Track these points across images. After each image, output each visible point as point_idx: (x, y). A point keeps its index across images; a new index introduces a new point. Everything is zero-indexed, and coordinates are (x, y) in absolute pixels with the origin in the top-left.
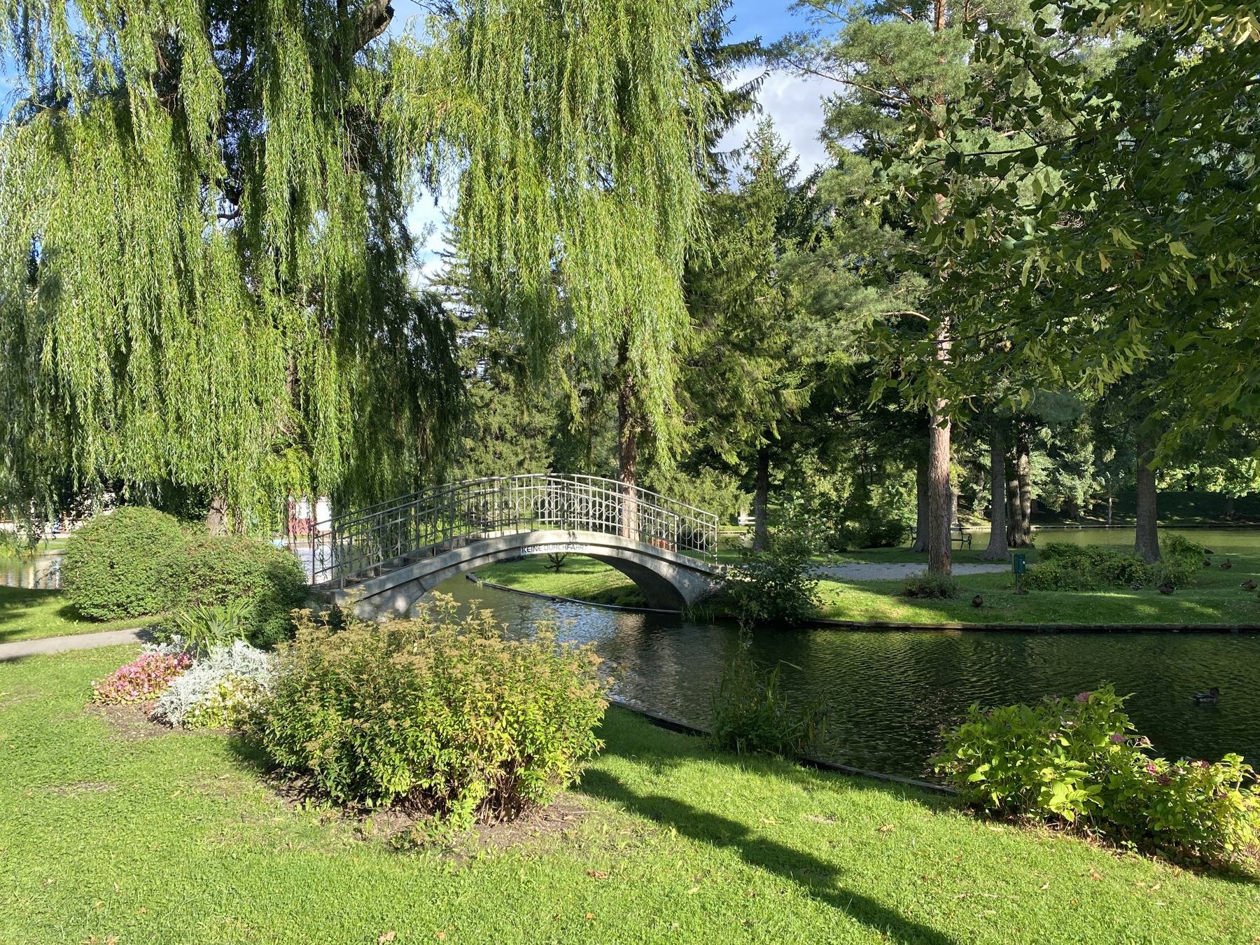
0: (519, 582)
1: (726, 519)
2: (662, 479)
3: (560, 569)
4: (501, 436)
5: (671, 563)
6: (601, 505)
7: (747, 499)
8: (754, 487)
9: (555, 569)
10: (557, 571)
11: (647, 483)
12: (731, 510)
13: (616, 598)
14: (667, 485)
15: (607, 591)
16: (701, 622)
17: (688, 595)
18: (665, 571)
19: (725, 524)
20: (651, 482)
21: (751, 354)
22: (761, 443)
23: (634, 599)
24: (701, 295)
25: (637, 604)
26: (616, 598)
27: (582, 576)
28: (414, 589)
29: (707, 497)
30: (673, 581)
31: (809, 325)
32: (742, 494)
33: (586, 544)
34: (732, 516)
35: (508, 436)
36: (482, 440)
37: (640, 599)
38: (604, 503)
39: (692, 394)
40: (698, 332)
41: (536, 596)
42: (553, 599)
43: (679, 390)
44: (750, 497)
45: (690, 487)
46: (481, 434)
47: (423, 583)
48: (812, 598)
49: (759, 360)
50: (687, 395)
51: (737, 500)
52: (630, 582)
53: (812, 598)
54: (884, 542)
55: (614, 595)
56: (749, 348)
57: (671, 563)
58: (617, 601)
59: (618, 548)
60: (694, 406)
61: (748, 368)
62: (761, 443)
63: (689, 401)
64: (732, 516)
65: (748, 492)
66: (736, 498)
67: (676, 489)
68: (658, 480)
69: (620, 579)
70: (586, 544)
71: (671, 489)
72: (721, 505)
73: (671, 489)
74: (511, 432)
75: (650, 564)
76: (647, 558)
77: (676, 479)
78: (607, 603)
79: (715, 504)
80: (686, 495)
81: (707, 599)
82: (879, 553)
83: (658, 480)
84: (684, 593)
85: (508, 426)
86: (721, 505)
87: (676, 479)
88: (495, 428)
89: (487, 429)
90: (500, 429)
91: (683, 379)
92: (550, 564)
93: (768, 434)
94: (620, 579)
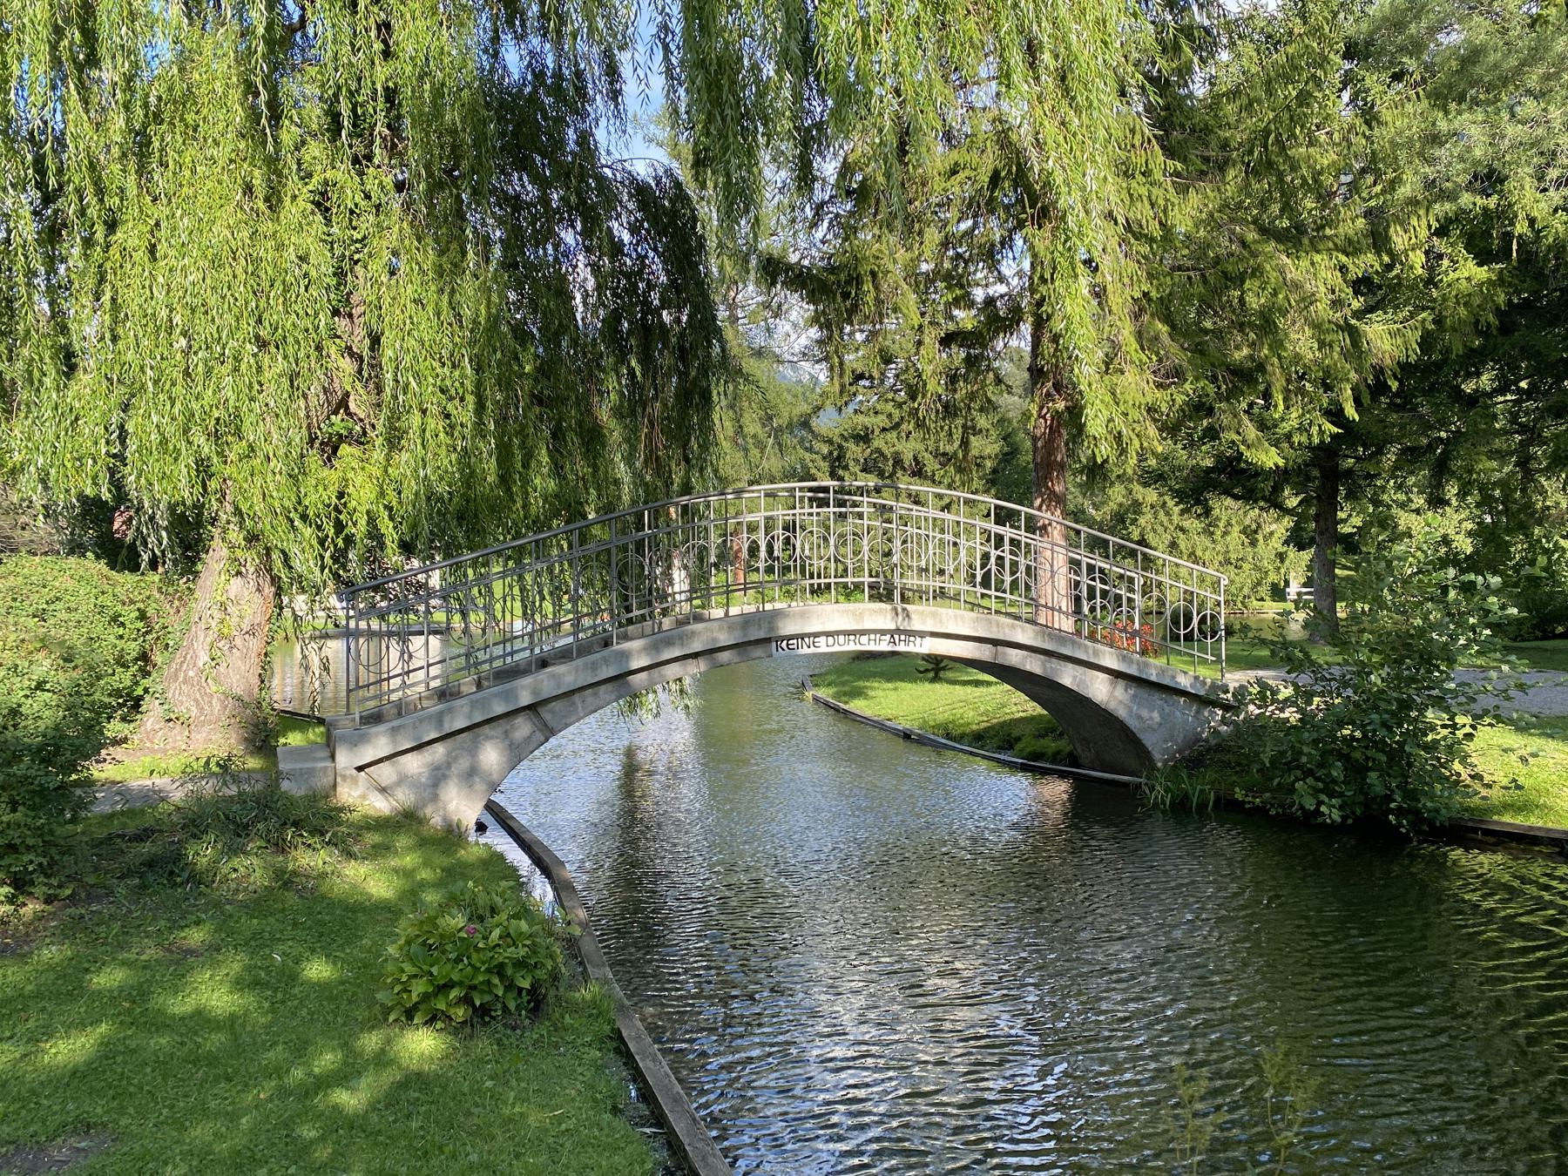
0: (866, 697)
1: (1264, 591)
2: (1160, 530)
3: (942, 674)
4: (918, 472)
5: (1116, 675)
6: (1014, 564)
7: (1299, 562)
8: (1312, 542)
9: (931, 675)
10: (936, 679)
11: (1136, 536)
12: (1272, 577)
13: (1018, 739)
14: (1167, 538)
15: (1003, 725)
16: (1182, 811)
17: (1160, 747)
18: (1099, 689)
19: (1262, 599)
20: (1142, 535)
21: (1298, 245)
22: (1321, 432)
23: (1050, 745)
24: (1193, 131)
25: (1056, 758)
26: (1018, 739)
27: (969, 689)
28: (523, 728)
29: (1233, 556)
30: (1122, 713)
31: (1443, 125)
32: (1292, 553)
33: (922, 634)
34: (1274, 587)
35: (928, 469)
36: (891, 476)
37: (1063, 745)
38: (994, 554)
39: (1173, 327)
40: (1183, 190)
41: (880, 726)
42: (907, 736)
43: (1146, 318)
44: (1306, 555)
45: (1205, 541)
46: (889, 468)
47: (547, 716)
48: (1457, 766)
49: (1317, 258)
50: (1162, 328)
51: (1282, 561)
52: (1040, 710)
53: (1457, 766)
54: (1560, 629)
55: (1015, 733)
56: (1295, 238)
57: (1116, 675)
58: (1019, 746)
59: (995, 642)
60: (1176, 354)
61: (1292, 274)
62: (1321, 432)
63: (1165, 339)
64: (1274, 587)
65: (1301, 547)
66: (1281, 557)
67: (1183, 544)
68: (1155, 531)
69: (1019, 705)
70: (922, 634)
71: (1173, 545)
72: (1257, 568)
73: (1173, 545)
74: (931, 465)
75: (1068, 677)
76: (1055, 663)
77: (1182, 530)
78: (1000, 749)
79: (1246, 566)
80: (1199, 553)
81: (1197, 756)
82: (1554, 651)
83: (1155, 531)
84: (1149, 740)
85: (927, 455)
86: (1257, 568)
87: (1182, 530)
88: (908, 458)
89: (898, 462)
90: (915, 458)
91: (1154, 294)
92: (923, 665)
93: (1335, 414)
94: (1019, 705)
